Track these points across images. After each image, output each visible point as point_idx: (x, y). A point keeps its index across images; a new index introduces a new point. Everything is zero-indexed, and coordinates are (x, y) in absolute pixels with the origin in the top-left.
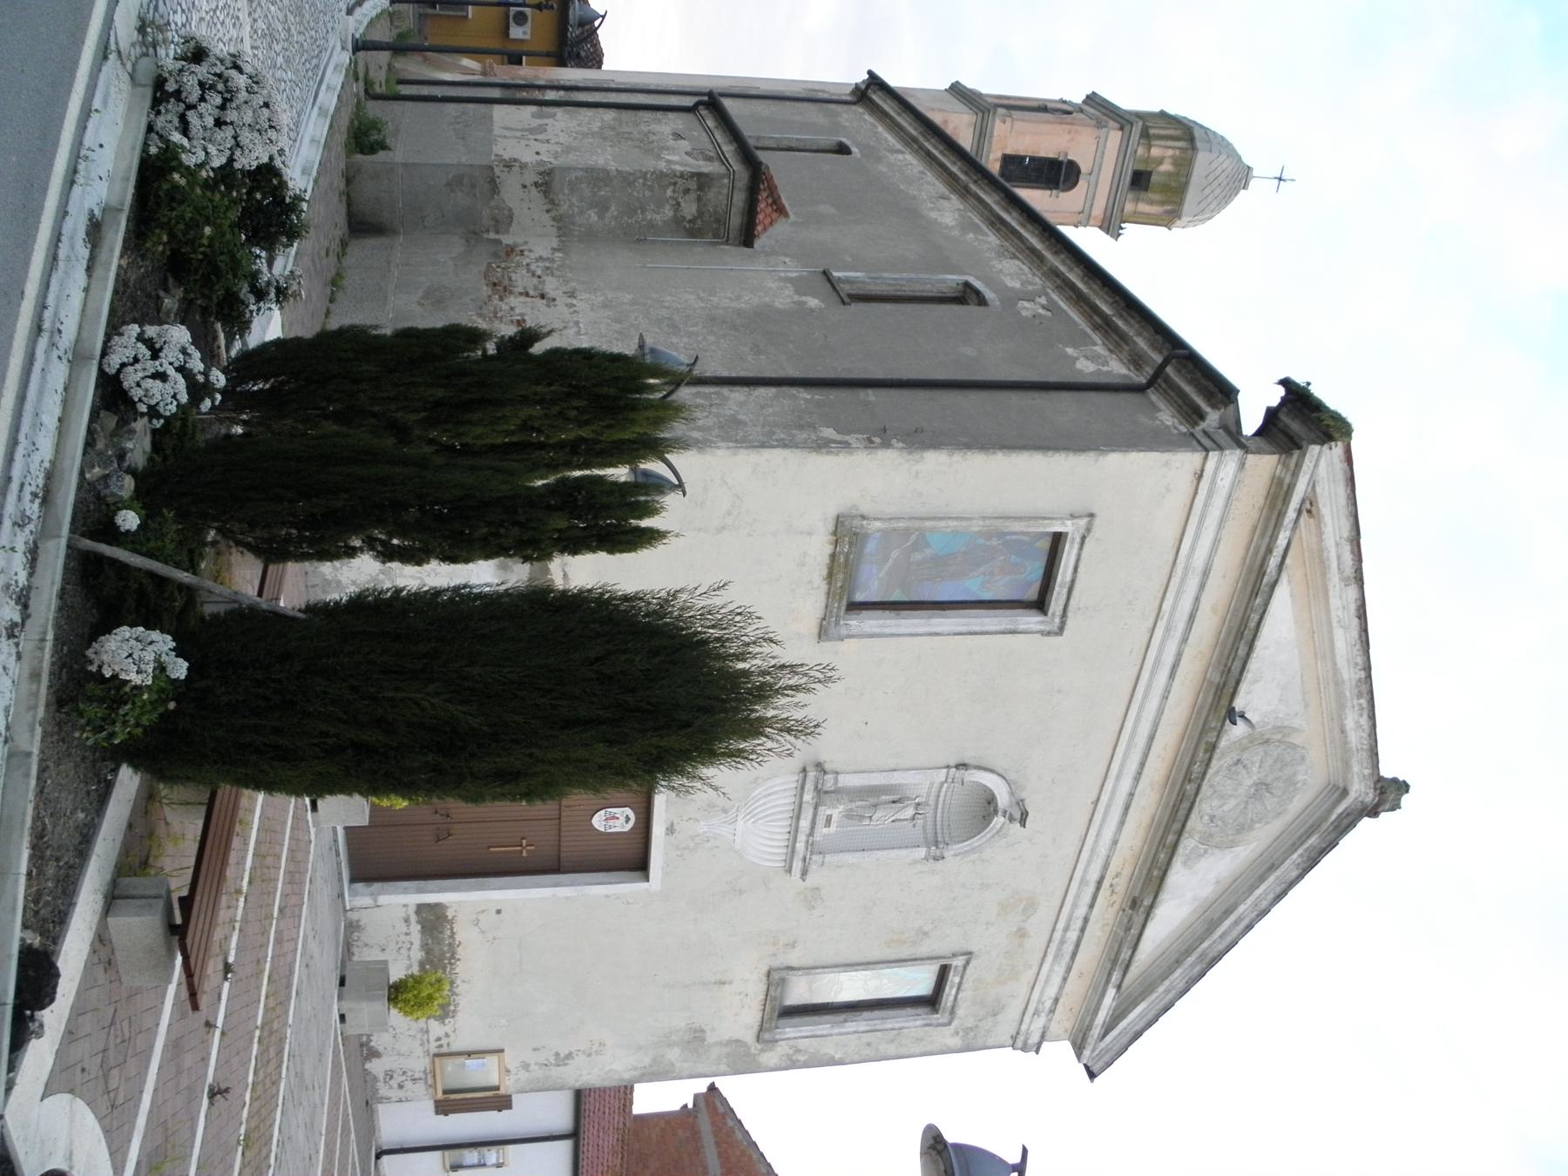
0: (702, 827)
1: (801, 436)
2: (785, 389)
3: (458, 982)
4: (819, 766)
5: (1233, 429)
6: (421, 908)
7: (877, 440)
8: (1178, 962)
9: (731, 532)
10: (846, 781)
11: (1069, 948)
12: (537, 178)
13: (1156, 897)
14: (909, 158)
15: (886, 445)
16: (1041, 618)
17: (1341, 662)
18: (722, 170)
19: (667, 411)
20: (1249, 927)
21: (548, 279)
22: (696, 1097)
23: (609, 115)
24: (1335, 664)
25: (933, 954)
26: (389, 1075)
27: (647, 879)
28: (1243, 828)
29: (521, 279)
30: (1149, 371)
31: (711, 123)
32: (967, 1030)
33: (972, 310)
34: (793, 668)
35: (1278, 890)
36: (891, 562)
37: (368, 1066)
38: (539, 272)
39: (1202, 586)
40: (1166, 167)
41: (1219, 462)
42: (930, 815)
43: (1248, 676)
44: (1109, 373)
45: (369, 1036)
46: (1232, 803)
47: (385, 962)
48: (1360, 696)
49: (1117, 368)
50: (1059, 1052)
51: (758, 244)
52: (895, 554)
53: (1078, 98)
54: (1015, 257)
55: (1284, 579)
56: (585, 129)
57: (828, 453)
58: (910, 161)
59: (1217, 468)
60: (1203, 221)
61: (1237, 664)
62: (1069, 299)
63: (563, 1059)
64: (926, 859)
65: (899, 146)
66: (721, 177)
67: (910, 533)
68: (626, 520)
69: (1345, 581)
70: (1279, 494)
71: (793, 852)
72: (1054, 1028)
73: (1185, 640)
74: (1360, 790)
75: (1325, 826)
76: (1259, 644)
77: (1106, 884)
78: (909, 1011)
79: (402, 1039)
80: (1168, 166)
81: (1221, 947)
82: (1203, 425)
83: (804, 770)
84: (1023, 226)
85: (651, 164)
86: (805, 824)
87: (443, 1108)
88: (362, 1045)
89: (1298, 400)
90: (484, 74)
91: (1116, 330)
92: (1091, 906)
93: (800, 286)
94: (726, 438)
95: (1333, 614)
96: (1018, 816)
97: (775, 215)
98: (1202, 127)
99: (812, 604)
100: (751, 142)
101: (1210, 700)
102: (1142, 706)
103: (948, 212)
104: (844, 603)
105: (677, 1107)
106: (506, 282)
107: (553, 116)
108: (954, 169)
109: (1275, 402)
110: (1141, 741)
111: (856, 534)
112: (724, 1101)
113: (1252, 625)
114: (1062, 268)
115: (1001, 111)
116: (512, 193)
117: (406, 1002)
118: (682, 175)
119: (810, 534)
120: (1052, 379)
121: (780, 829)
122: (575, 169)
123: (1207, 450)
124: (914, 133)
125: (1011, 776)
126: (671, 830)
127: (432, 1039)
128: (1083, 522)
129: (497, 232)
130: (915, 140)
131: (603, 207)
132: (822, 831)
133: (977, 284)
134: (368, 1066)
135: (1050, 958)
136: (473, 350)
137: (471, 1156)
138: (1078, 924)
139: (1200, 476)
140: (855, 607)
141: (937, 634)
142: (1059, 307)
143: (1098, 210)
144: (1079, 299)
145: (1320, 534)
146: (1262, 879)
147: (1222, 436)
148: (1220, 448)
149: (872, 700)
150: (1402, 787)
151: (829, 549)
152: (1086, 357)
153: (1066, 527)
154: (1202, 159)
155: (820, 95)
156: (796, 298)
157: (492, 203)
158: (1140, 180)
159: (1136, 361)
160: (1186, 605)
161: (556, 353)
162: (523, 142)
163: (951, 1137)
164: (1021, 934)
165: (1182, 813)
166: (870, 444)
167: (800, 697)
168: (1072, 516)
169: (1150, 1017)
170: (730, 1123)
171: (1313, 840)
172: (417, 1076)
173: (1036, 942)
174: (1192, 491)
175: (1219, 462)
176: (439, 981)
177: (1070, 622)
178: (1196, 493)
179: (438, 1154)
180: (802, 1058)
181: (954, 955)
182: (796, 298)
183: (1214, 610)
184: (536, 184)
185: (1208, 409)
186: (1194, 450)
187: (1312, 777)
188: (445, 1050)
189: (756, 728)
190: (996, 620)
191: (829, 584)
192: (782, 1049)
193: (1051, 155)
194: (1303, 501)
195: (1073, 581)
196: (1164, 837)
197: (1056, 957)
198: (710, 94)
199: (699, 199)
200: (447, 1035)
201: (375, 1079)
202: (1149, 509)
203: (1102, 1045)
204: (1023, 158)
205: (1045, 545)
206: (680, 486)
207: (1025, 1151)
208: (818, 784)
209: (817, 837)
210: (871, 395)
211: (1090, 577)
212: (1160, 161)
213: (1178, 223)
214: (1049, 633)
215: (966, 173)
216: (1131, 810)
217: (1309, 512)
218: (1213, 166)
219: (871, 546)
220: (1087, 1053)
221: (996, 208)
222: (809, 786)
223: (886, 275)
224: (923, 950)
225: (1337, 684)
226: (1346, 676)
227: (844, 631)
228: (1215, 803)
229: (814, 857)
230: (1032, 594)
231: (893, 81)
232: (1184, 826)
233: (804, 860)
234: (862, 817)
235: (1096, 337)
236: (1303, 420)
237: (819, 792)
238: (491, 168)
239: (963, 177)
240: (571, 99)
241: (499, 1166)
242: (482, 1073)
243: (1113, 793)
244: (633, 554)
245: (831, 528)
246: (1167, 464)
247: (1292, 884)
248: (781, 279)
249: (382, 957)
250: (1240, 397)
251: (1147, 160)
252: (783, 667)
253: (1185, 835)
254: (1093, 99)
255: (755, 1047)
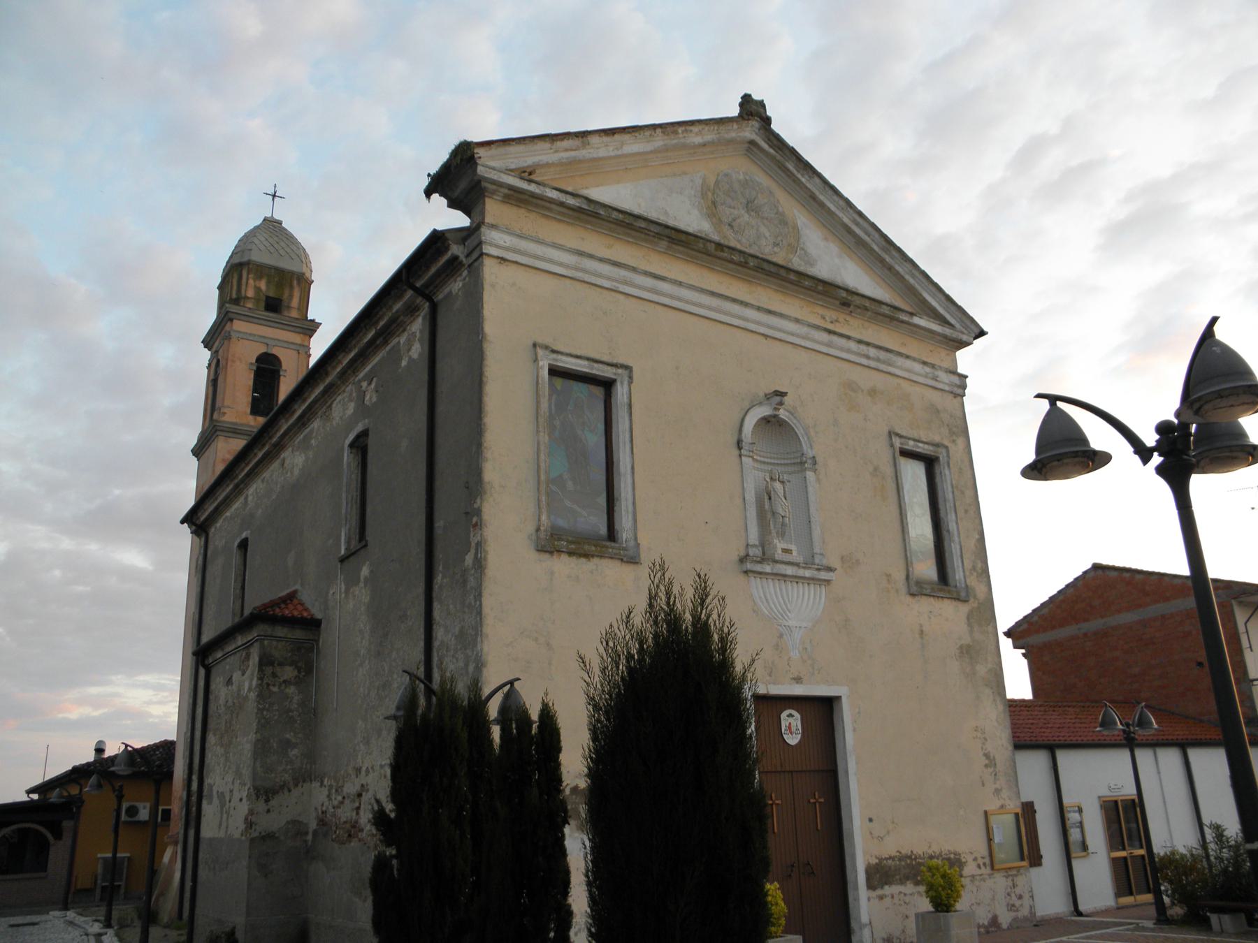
0: (795, 655)
1: (472, 582)
2: (434, 595)
3: (930, 852)
4: (742, 560)
5: (465, 234)
6: (871, 886)
7: (475, 520)
8: (890, 268)
9: (546, 641)
10: (754, 537)
11: (882, 355)
12: (262, 801)
13: (839, 287)
14: (251, 491)
15: (478, 512)
16: (618, 384)
17: (648, 147)
18: (257, 645)
19: (444, 699)
20: (860, 214)
21: (346, 790)
22: (1015, 647)
23: (212, 739)
24: (651, 152)
25: (892, 462)
26: (1011, 907)
27: (838, 698)
28: (783, 221)
29: (346, 813)
30: (419, 300)
31: (219, 654)
32: (952, 433)
33: (372, 441)
34: (652, 598)
35: (830, 192)
36: (575, 507)
37: (1005, 926)
38: (340, 798)
39: (591, 256)
40: (263, 285)
41: (492, 245)
42: (780, 469)
43: (663, 219)
44: (421, 332)
45: (979, 926)
46: (763, 229)
47: (917, 915)
48: (676, 133)
49: (418, 326)
50: (965, 359)
51: (319, 616)
52: (568, 503)
53: (207, 354)
54: (330, 406)
55: (585, 192)
56: (222, 760)
57: (485, 559)
58: (254, 490)
59: (497, 246)
60: (306, 255)
61: (653, 228)
62: (363, 365)
63: (990, 761)
64: (815, 471)
65: (242, 499)
66: (262, 647)
67: (549, 491)
68: (532, 738)
69: (585, 145)
70: (516, 197)
71: (813, 579)
72: (946, 365)
73: (634, 270)
74: (750, 131)
75: (778, 157)
76: (636, 211)
77: (831, 327)
78: (938, 479)
79: (981, 897)
80: (263, 280)
81: (877, 235)
82: (462, 257)
83: (746, 572)
84: (305, 400)
85: (251, 705)
86: (790, 570)
87: (1035, 859)
88: (988, 932)
89: (440, 184)
90: (176, 843)
91: (387, 326)
92: (849, 338)
93: (352, 581)
94: (474, 643)
95: (612, 154)
96: (778, 399)
97: (295, 601)
98: (231, 257)
99: (610, 570)
100: (237, 620)
101: (681, 249)
102: (687, 302)
103: (295, 460)
104: (608, 544)
105: (1025, 662)
106: (348, 826)
107: (211, 786)
108: (260, 455)
109: (444, 201)
110: (715, 302)
111: (552, 535)
112: (1018, 624)
113: (621, 216)
114: (339, 369)
115: (215, 416)
116: (274, 821)
117: (949, 897)
118: (261, 679)
119: (552, 573)
120: (425, 377)
121: (794, 590)
122: (254, 768)
123: (482, 254)
124: (231, 487)
125: (747, 404)
126: (798, 680)
127: (979, 872)
128: (540, 352)
129: (307, 833)
130: (237, 486)
131: (287, 745)
132: (796, 556)
133: (351, 437)
134: (1005, 926)
135: (891, 369)
136: (392, 867)
137: (1074, 835)
138: (863, 348)
139: (502, 260)
140: (612, 535)
141: (633, 468)
142: (370, 371)
143: (297, 338)
144: (363, 356)
145: (548, 165)
146: (822, 205)
147: (471, 243)
148: (480, 243)
149: (687, 521)
150: (746, 99)
151: (564, 557)
152: (409, 350)
153: (544, 365)
154: (257, 257)
155: (200, 562)
156: (362, 585)
157: (282, 838)
158: (273, 305)
159: (411, 310)
160: (606, 269)
161: (395, 795)
162: (232, 812)
163: (1030, 457)
164: (873, 392)
165: (773, 269)
166: (478, 526)
167: (676, 590)
168: (536, 360)
169: (934, 289)
170: (1036, 618)
171: (790, 166)
172: (1010, 883)
173: (878, 380)
174: (514, 266)
175: (492, 245)
176: (930, 869)
177: (621, 361)
178: (516, 263)
179: (1075, 863)
180: (979, 565)
181: (892, 445)
182: (362, 585)
183: (610, 247)
184: (267, 801)
185: (449, 253)
186: (482, 264)
187: (741, 168)
188: (987, 861)
189: (702, 628)
190: (620, 420)
191: (593, 556)
192: (972, 581)
193: (252, 376)
194: (522, 178)
195: (588, 359)
196: (791, 282)
197: (890, 365)
198: (195, 654)
199: (281, 664)
200: (975, 859)
201: (1015, 919)
202: (528, 303)
203: (958, 325)
204: (254, 398)
205: (559, 382)
206: (511, 683)
207: (1039, 396)
208: (754, 562)
209: (800, 560)
210: (439, 524)
211: (584, 345)
212: (258, 289)
213: (307, 275)
214: (631, 377)
215: (264, 445)
216: (770, 308)
217: (530, 174)
218: (262, 248)
219: (561, 523)
220: (965, 338)
221: (291, 422)
222: (758, 568)
223: (344, 511)
224: (889, 471)
225: (667, 150)
226: (661, 143)
227: (632, 543)
228: (763, 242)
229: (817, 561)
230: (599, 392)
231: (190, 502)
232: (782, 267)
233: (819, 570)
234: (783, 524)
235: (394, 342)
236: (458, 177)
237: (762, 560)
238: (252, 840)
239: (266, 448)
240: (197, 768)
241: (1080, 810)
242: (1004, 830)
243: (758, 323)
244: (562, 731)
245: (547, 556)
246: (493, 286)
247: (825, 182)
248: (346, 597)
249: (913, 918)
250: (439, 228)
251: (257, 300)
252: (651, 605)
253: (790, 266)
254: (208, 343)
255: (973, 604)
